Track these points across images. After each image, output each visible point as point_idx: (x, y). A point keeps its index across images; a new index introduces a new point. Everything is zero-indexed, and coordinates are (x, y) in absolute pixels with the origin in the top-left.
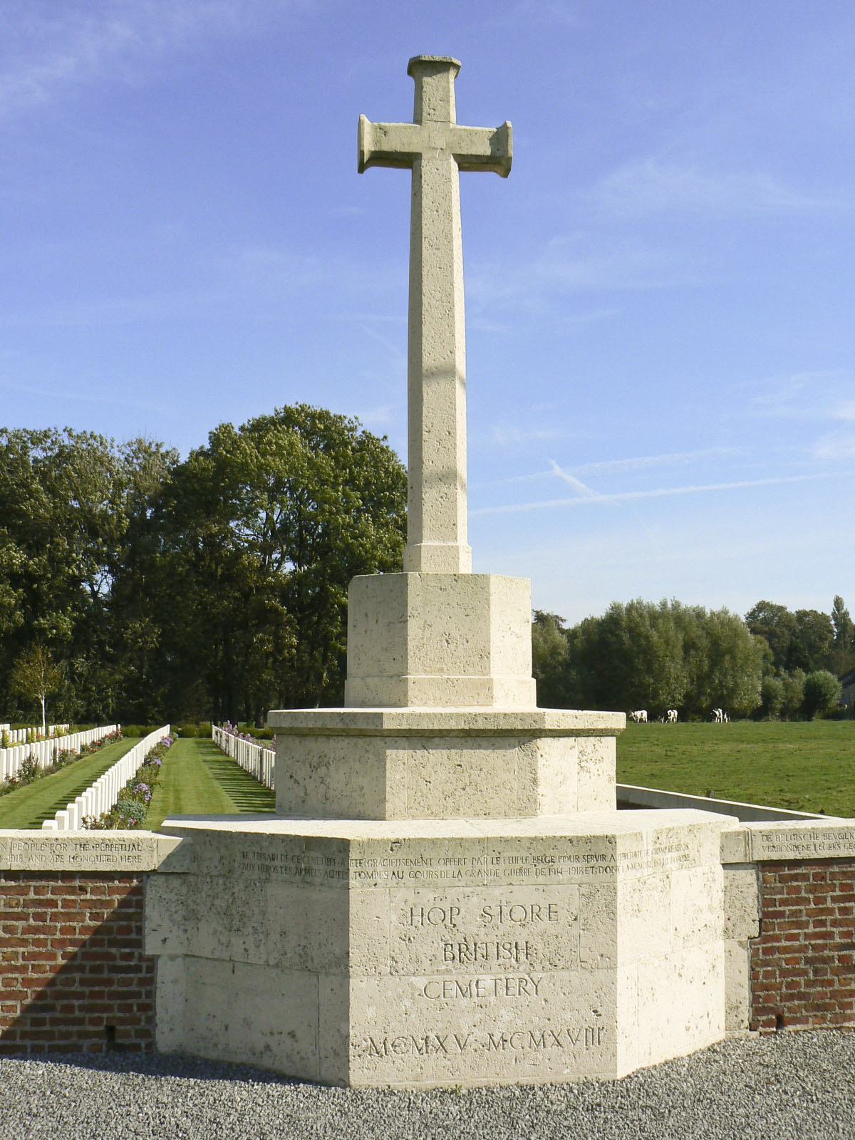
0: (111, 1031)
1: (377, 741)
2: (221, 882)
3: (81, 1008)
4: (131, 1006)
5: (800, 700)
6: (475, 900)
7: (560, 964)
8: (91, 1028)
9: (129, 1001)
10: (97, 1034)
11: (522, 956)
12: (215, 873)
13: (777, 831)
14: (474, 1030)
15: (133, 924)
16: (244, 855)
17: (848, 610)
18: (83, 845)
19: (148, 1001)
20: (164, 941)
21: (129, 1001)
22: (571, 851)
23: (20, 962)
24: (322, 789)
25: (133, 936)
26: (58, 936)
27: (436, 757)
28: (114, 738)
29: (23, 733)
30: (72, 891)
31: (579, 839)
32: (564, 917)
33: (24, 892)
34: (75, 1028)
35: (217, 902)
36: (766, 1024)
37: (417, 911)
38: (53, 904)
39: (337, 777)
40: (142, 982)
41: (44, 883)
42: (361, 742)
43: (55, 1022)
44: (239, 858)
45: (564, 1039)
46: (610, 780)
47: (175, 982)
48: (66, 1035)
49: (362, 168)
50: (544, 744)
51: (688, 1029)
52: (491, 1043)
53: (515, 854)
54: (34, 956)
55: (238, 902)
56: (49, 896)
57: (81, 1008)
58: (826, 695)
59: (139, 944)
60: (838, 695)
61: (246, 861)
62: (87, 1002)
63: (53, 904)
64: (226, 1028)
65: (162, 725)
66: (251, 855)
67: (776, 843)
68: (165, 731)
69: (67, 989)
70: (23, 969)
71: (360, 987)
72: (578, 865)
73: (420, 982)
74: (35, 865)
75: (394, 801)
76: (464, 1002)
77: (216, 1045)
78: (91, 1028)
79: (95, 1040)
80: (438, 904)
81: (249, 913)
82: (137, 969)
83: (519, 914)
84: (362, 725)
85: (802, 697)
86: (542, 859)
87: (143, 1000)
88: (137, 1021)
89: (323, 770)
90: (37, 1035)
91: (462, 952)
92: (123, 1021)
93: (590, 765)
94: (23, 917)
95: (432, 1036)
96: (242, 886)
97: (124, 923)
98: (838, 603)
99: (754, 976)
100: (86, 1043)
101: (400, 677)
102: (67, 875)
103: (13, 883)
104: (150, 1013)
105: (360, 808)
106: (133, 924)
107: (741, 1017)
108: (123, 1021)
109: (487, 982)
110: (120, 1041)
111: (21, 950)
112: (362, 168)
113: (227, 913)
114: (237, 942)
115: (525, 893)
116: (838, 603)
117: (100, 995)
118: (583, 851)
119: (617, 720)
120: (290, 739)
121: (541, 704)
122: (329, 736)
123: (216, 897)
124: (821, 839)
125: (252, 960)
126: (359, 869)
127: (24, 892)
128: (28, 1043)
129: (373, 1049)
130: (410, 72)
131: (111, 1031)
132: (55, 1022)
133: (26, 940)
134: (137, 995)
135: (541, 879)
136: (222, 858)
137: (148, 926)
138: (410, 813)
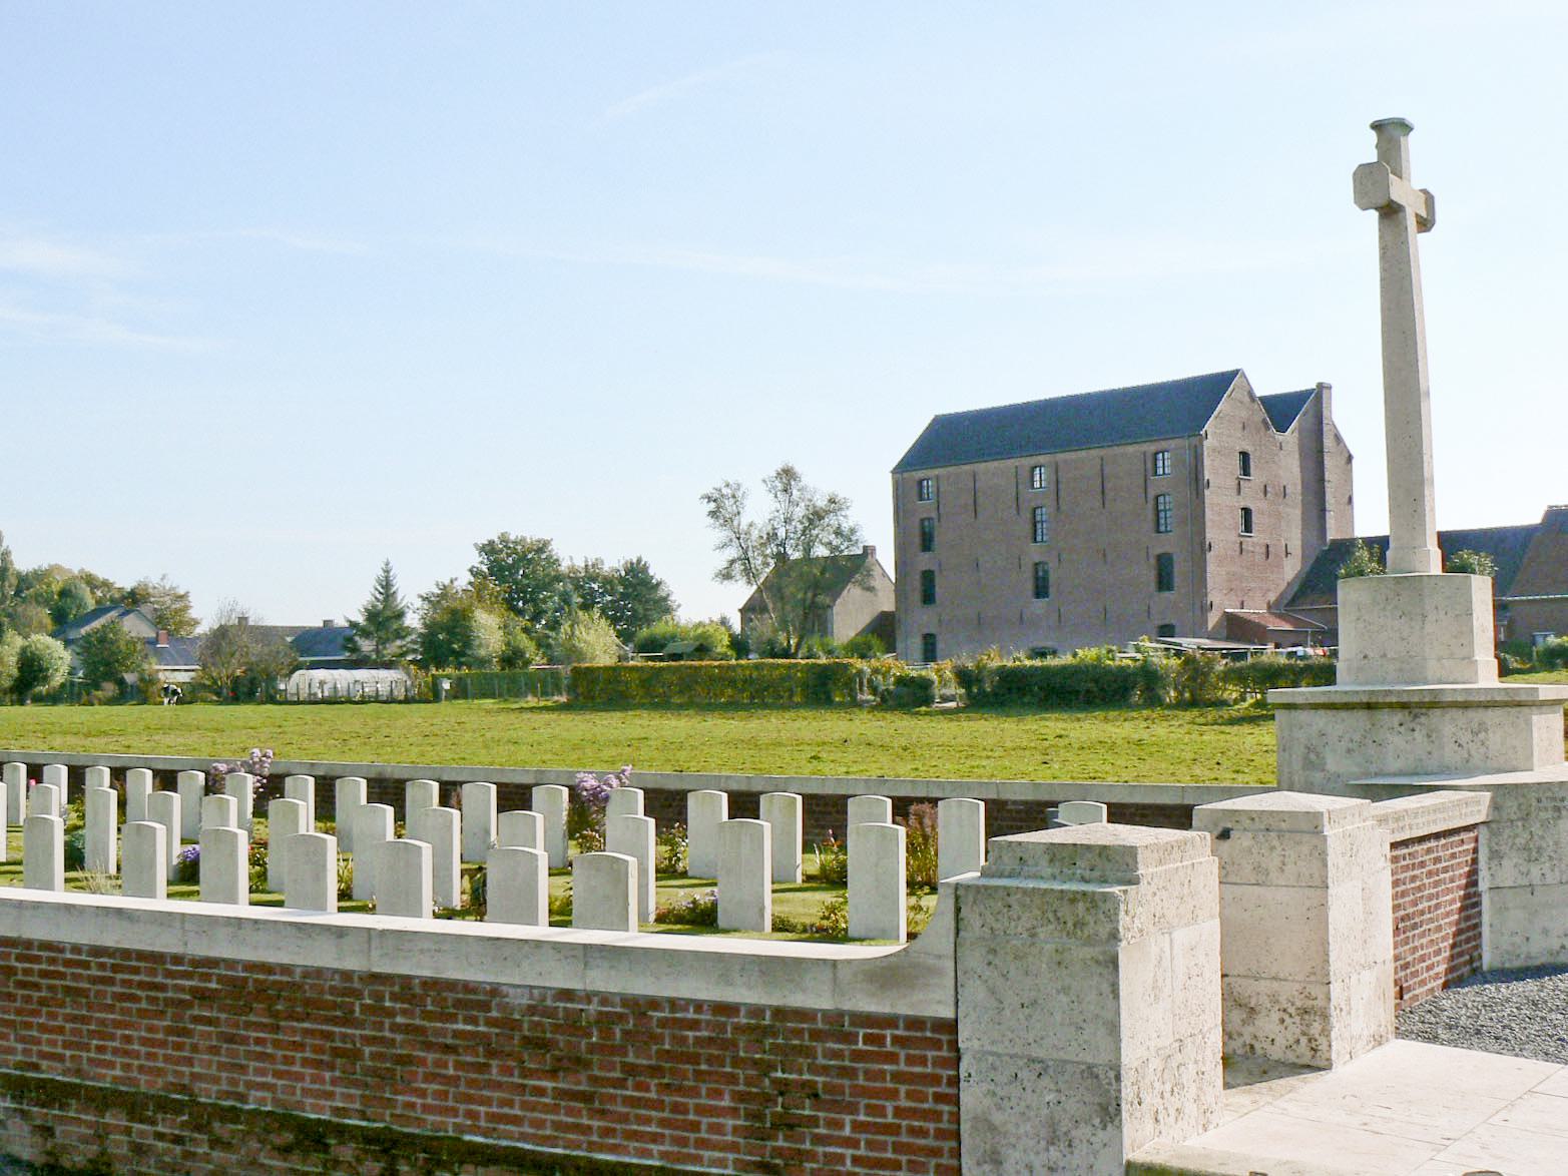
1: (1525, 710)
2: (1520, 824)
5: (10, 676)
12: (1514, 817)
16: (1539, 801)
17: (10, 548)
24: (1483, 750)
35: (1517, 841)
39: (1494, 739)
42: (1514, 711)
44: (1534, 803)
55: (1536, 837)
58: (48, 669)
60: (64, 669)
61: (1540, 805)
64: (1528, 939)
66: (1543, 799)
77: (1519, 956)
81: (1544, 845)
84: (1523, 697)
85: (15, 672)
89: (1482, 735)
96: (1538, 825)
105: (1514, 763)
113: (1526, 848)
114: (1535, 871)
120: (1448, 717)
122: (1486, 707)
123: (1516, 836)
125: (1549, 880)
136: (1520, 805)
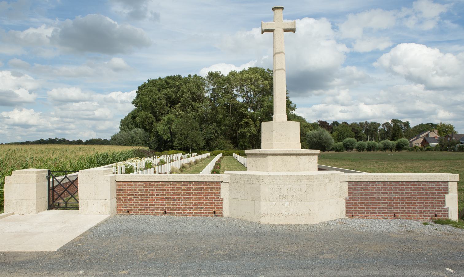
0: (215, 212)
3: (209, 208)
4: (218, 207)
6: (285, 187)
7: (303, 200)
8: (211, 212)
9: (218, 207)
10: (212, 213)
11: (295, 198)
13: (352, 175)
14: (285, 212)
15: (219, 192)
18: (209, 176)
19: (222, 207)
20: (225, 195)
21: (218, 207)
22: (305, 178)
23: (197, 199)
25: (219, 194)
26: (204, 194)
28: (208, 157)
29: (186, 155)
31: (307, 175)
34: (208, 212)
36: (349, 216)
37: (274, 189)
38: (203, 188)
40: (221, 203)
41: (201, 184)
43: (204, 210)
45: (304, 215)
46: (316, 164)
47: (227, 203)
48: (206, 213)
49: (262, 33)
51: (331, 215)
52: (288, 215)
53: (293, 178)
56: (202, 186)
57: (209, 208)
59: (220, 196)
62: (210, 207)
65: (195, 153)
67: (352, 178)
68: (221, 155)
69: (206, 204)
70: (197, 200)
72: (306, 180)
73: (274, 203)
76: (283, 207)
78: (211, 212)
79: (212, 214)
80: (278, 188)
83: (294, 190)
86: (299, 179)
87: (221, 206)
88: (220, 210)
90: (200, 213)
91: (283, 197)
92: (217, 210)
93: (311, 161)
94: (197, 190)
95: (277, 213)
97: (217, 192)
100: (210, 215)
102: (206, 182)
103: (195, 184)
104: (222, 209)
106: (219, 192)
107: (344, 214)
108: (217, 210)
109: (288, 203)
110: (216, 214)
111: (197, 197)
112: (262, 33)
117: (213, 205)
118: (307, 178)
119: (318, 151)
121: (302, 148)
124: (362, 177)
126: (262, 181)
127: (198, 185)
128: (199, 214)
129: (265, 216)
130: (272, 10)
131: (215, 212)
132: (204, 210)
133: (198, 195)
134: (220, 205)
135: (299, 183)
138: (264, 148)
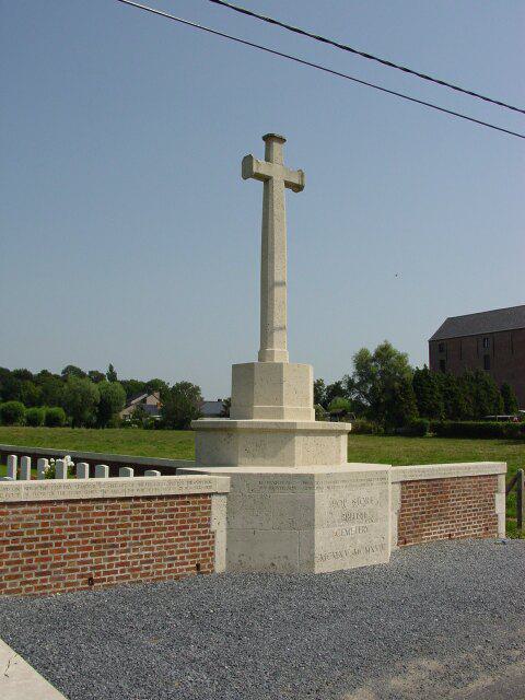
10: (193, 568)
27: (311, 439)
30: (184, 503)
32: (375, 502)
33: (165, 505)
40: (210, 543)
50: (298, 439)
54: (169, 535)
59: (209, 526)
63: (176, 510)
71: (318, 533)
74: (172, 493)
75: (299, 457)
82: (209, 537)
91: (347, 518)
92: (203, 561)
98: (111, 368)
99: (399, 525)
101: (279, 400)
102: (183, 496)
115: (363, 493)
116: (111, 368)
131: (198, 566)
132: (177, 564)
134: (208, 549)
137: (213, 517)
